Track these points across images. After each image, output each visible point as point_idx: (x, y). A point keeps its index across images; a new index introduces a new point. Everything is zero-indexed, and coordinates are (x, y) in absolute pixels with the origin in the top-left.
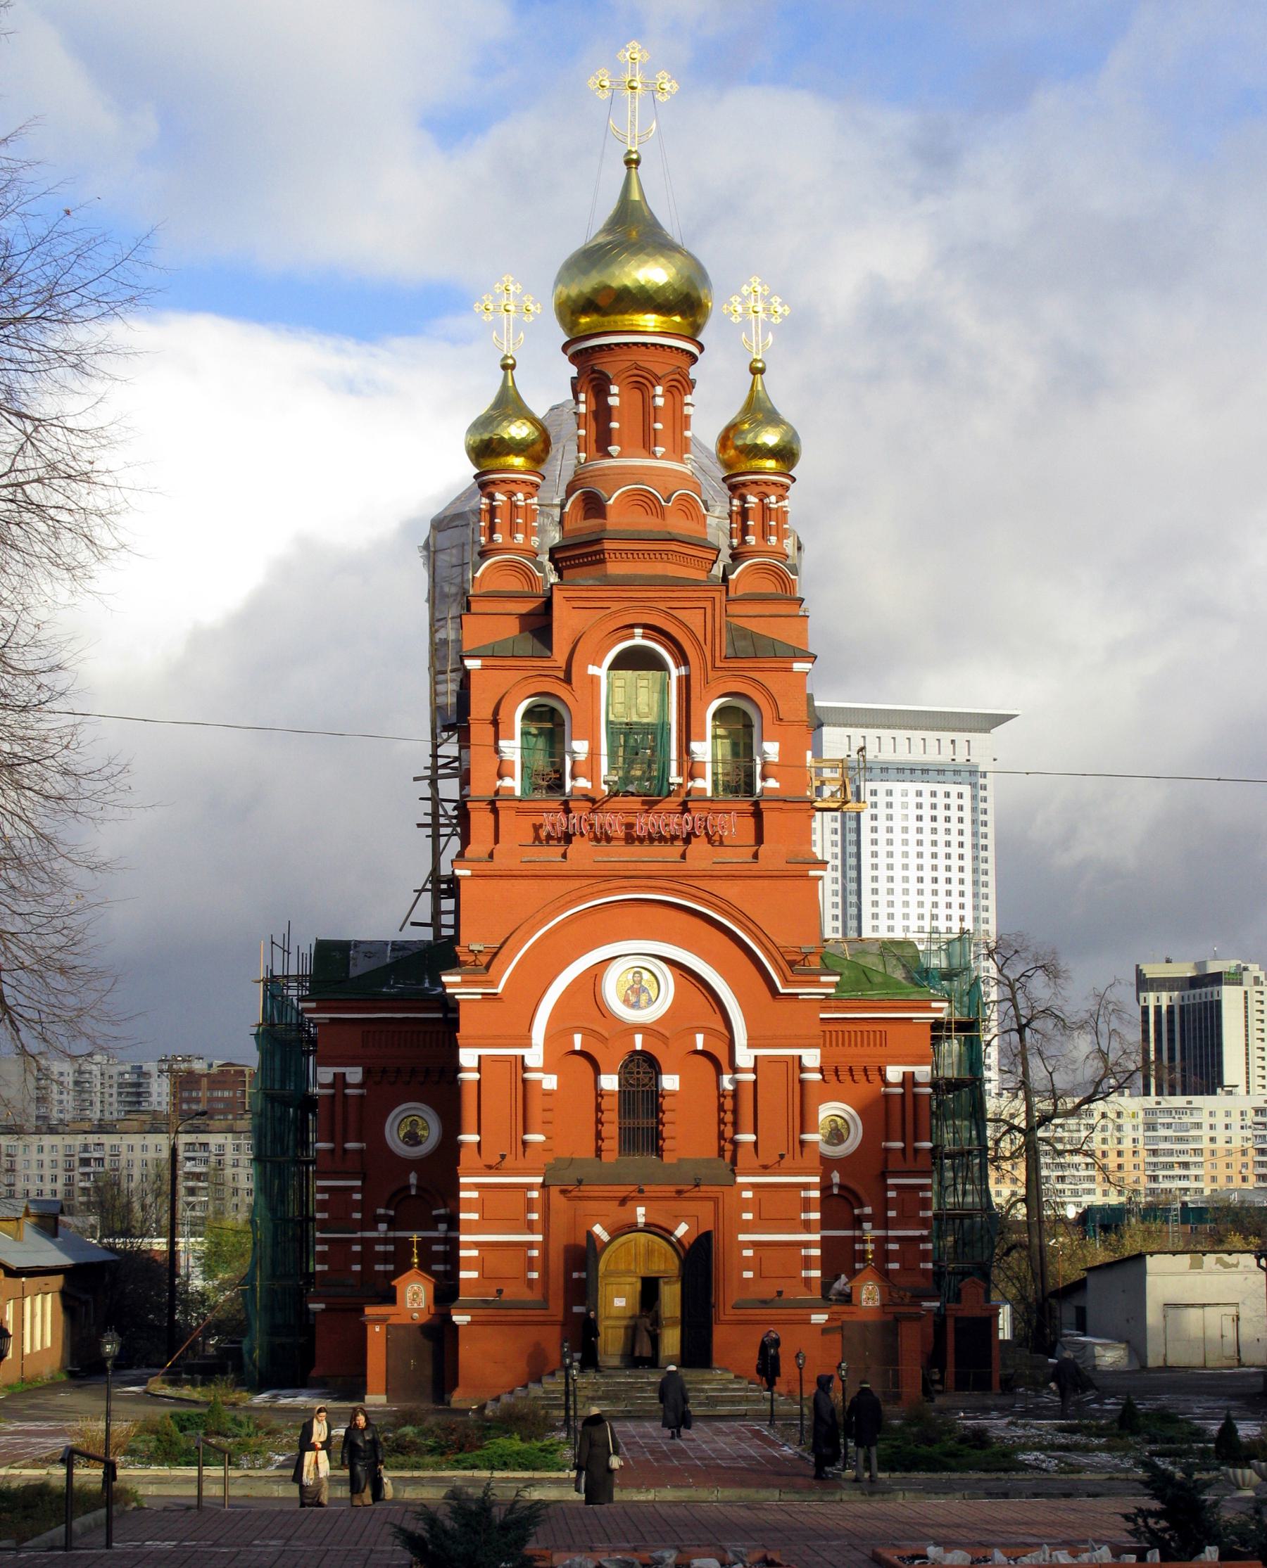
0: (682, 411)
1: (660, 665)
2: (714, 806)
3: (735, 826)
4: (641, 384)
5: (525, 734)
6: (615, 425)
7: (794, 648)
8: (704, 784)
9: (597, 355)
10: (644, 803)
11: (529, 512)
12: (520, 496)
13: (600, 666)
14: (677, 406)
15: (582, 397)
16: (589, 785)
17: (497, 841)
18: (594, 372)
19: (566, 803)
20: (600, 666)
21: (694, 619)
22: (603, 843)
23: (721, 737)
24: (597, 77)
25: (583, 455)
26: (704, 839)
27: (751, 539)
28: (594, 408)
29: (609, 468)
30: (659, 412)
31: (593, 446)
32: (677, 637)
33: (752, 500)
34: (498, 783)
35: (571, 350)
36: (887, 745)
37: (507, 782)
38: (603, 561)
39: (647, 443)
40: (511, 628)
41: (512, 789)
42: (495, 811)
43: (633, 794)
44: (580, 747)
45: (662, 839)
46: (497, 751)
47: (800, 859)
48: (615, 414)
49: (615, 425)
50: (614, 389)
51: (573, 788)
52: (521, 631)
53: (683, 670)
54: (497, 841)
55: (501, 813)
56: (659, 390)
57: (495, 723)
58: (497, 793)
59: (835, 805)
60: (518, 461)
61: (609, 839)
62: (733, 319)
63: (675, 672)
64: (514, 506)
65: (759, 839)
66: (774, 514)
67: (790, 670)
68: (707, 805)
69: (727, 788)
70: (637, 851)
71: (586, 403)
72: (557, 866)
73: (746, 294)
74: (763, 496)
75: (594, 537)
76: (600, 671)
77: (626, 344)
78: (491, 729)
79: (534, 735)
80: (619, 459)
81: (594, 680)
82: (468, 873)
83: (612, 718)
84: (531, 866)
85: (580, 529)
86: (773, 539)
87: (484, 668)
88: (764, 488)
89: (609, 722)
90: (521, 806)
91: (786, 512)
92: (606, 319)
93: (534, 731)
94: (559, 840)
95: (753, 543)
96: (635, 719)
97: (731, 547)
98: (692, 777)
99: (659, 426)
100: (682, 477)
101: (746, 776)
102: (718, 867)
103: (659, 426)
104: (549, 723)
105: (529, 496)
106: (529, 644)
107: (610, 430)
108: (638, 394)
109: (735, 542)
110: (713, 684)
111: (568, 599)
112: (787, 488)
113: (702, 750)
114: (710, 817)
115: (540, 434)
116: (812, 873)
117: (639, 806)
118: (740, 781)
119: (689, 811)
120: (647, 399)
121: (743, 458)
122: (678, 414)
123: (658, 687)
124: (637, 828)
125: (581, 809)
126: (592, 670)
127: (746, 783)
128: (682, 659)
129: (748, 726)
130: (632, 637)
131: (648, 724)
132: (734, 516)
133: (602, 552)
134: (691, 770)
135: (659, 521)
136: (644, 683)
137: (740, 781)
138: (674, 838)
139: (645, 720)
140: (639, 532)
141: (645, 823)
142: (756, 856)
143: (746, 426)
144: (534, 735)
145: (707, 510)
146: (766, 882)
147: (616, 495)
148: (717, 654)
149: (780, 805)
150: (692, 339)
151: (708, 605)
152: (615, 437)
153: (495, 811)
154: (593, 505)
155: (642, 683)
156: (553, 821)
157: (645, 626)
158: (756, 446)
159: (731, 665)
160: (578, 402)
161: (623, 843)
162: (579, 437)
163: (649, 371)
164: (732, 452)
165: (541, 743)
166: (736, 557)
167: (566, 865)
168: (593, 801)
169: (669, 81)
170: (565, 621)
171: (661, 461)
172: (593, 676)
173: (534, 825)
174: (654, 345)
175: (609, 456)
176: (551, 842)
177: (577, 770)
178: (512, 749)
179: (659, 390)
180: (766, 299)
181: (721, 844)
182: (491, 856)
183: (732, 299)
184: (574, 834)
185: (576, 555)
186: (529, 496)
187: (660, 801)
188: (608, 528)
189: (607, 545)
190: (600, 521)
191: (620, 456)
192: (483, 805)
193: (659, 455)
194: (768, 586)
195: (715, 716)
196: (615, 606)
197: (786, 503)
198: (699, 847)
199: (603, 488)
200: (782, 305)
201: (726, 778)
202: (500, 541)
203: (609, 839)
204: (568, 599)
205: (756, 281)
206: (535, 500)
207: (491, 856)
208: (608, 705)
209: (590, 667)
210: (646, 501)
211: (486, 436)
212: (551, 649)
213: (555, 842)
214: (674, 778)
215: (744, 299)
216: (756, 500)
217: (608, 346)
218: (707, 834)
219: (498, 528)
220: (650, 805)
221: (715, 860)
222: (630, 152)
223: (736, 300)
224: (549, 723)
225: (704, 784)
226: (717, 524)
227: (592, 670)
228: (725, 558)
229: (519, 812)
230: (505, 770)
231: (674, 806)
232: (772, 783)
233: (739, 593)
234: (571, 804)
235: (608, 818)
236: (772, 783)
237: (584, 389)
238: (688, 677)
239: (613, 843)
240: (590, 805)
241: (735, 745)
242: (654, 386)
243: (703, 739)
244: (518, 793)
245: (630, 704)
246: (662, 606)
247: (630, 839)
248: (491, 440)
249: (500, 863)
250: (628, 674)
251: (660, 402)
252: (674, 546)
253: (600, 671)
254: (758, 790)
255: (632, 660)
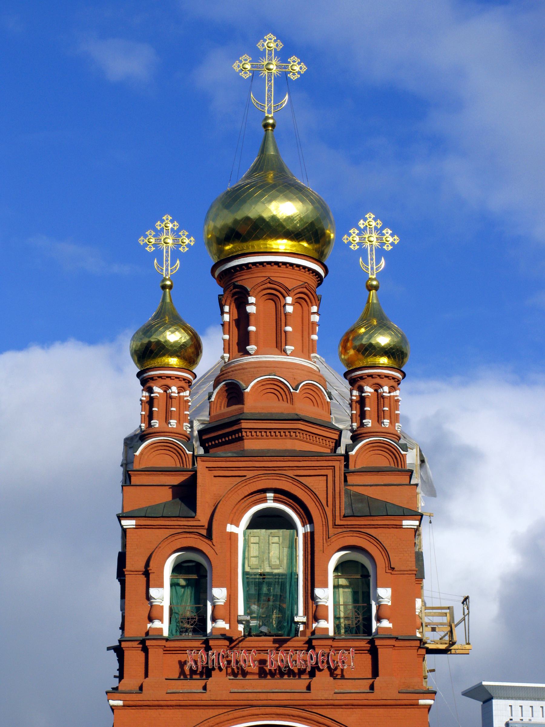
0: (309, 319)
1: (290, 525)
2: (335, 644)
3: (355, 663)
4: (275, 295)
5: (173, 585)
6: (252, 328)
7: (404, 508)
8: (328, 625)
9: (238, 274)
10: (275, 641)
11: (183, 404)
12: (174, 389)
13: (237, 525)
14: (306, 314)
15: (227, 309)
16: (227, 626)
17: (146, 675)
18: (236, 287)
19: (206, 642)
20: (237, 525)
21: (318, 485)
22: (240, 677)
23: (343, 587)
24: (241, 62)
25: (227, 355)
26: (326, 672)
27: (368, 422)
28: (236, 317)
29: (247, 364)
30: (288, 317)
31: (235, 348)
32: (292, 491)
33: (369, 390)
34: (149, 625)
35: (217, 273)
36: (538, 712)
37: (157, 624)
38: (241, 439)
39: (279, 343)
40: (166, 495)
41: (161, 630)
42: (145, 650)
43: (266, 635)
44: (220, 594)
45: (291, 673)
46: (148, 597)
47: (411, 690)
48: (252, 319)
49: (252, 328)
50: (252, 300)
51: (213, 628)
52: (174, 497)
53: (308, 528)
54: (146, 675)
55: (151, 651)
56: (289, 300)
57: (147, 574)
58: (147, 633)
59: (443, 647)
60: (174, 361)
61: (245, 674)
62: (352, 247)
63: (301, 530)
64: (170, 397)
65: (375, 673)
66: (387, 401)
67: (400, 526)
68: (330, 642)
69: (348, 630)
70: (269, 684)
71: (229, 313)
72: (197, 697)
73: (159, 228)
74: (377, 387)
75: (233, 419)
76: (239, 530)
77: (261, 263)
78: (143, 579)
79: (183, 587)
80: (256, 356)
81: (233, 537)
82: (120, 703)
83: (247, 569)
84: (175, 697)
85: (223, 414)
86: (386, 422)
87: (138, 527)
88: (378, 380)
89: (245, 573)
90: (168, 646)
91: (398, 401)
92: (245, 245)
93: (183, 582)
94: (201, 674)
95: (157, 426)
96: (268, 570)
97: (352, 431)
98: (316, 619)
99: (289, 329)
100: (310, 371)
101: (364, 619)
102: (339, 696)
103: (289, 329)
104: (195, 576)
105: (181, 389)
106: (180, 507)
107: (248, 333)
108: (272, 304)
109: (355, 425)
110: (333, 539)
111: (210, 469)
112: (398, 382)
113: (325, 595)
114: (332, 653)
115: (191, 339)
116: (421, 702)
117: (271, 644)
118: (359, 623)
119: (313, 648)
120: (279, 307)
121: (360, 356)
122: (306, 320)
123: (287, 543)
124: (268, 663)
125: (219, 647)
126: (230, 528)
127: (364, 625)
128: (307, 518)
129: (366, 576)
130: (265, 500)
131: (279, 575)
132: (354, 404)
133: (240, 430)
134: (315, 613)
135: (289, 405)
136: (276, 539)
137: (359, 623)
138: (301, 672)
139: (276, 571)
140: (271, 414)
141: (276, 659)
142: (372, 687)
143: (363, 330)
144: (183, 587)
145: (331, 399)
146: (381, 711)
147: (252, 384)
148: (337, 514)
149: (392, 642)
150: (319, 261)
151: (329, 473)
152: (252, 338)
153: (145, 650)
154: (234, 393)
155: (274, 541)
156: (195, 657)
157: (276, 491)
158: (371, 345)
159: (349, 523)
160: (222, 312)
161: (257, 677)
162: (224, 340)
163: (280, 285)
164: (352, 352)
165: (189, 592)
166: (356, 438)
167: (206, 696)
168: (230, 640)
169: (299, 64)
170: (208, 488)
171: (290, 358)
172: (231, 533)
173: (180, 662)
174: (285, 264)
175: (247, 353)
176: (195, 677)
177: (217, 613)
178: (162, 595)
179: (289, 300)
180: (379, 231)
181: (343, 677)
182: (141, 688)
183: (351, 231)
184: (213, 669)
185: (220, 435)
186: (181, 389)
187: (288, 640)
188: (246, 411)
189: (245, 425)
190: (241, 406)
191: (257, 353)
192: (135, 644)
193: (289, 352)
194: (382, 461)
195: (336, 569)
196: (249, 474)
197: (397, 393)
198: (322, 679)
199: (242, 380)
200: (392, 235)
201: (347, 622)
202: (157, 426)
203: (245, 674)
204: (210, 469)
205: (370, 216)
206: (187, 393)
207: (141, 688)
208: (244, 558)
209: (229, 526)
210: (277, 389)
211: (146, 341)
212: (195, 511)
213: (198, 677)
214: (300, 618)
215: (361, 232)
216: (372, 390)
217: (247, 265)
218: (329, 668)
219: (155, 415)
220: (280, 643)
221: (336, 691)
222: (267, 118)
223: (354, 231)
224: (195, 576)
225: (328, 625)
226: (342, 419)
227: (230, 528)
228: (346, 439)
229: (167, 651)
230: (154, 614)
231: (301, 644)
232: (386, 624)
233: (358, 467)
234: (211, 643)
235: (243, 655)
236: (386, 624)
237: (228, 301)
238: (312, 533)
239: (248, 677)
240: (227, 643)
241: (355, 594)
242: (284, 297)
243: (326, 585)
244: (166, 634)
245: (264, 555)
246: (290, 473)
247: (263, 673)
248: (150, 343)
249: (148, 695)
250: (263, 532)
251: (289, 309)
252: (300, 425)
253: (239, 530)
254: (374, 630)
255: (265, 521)
